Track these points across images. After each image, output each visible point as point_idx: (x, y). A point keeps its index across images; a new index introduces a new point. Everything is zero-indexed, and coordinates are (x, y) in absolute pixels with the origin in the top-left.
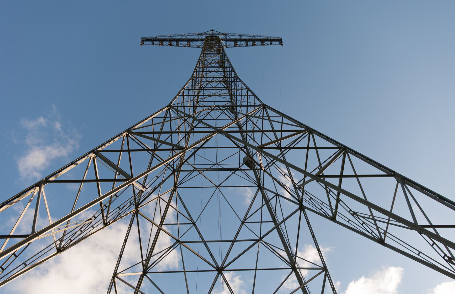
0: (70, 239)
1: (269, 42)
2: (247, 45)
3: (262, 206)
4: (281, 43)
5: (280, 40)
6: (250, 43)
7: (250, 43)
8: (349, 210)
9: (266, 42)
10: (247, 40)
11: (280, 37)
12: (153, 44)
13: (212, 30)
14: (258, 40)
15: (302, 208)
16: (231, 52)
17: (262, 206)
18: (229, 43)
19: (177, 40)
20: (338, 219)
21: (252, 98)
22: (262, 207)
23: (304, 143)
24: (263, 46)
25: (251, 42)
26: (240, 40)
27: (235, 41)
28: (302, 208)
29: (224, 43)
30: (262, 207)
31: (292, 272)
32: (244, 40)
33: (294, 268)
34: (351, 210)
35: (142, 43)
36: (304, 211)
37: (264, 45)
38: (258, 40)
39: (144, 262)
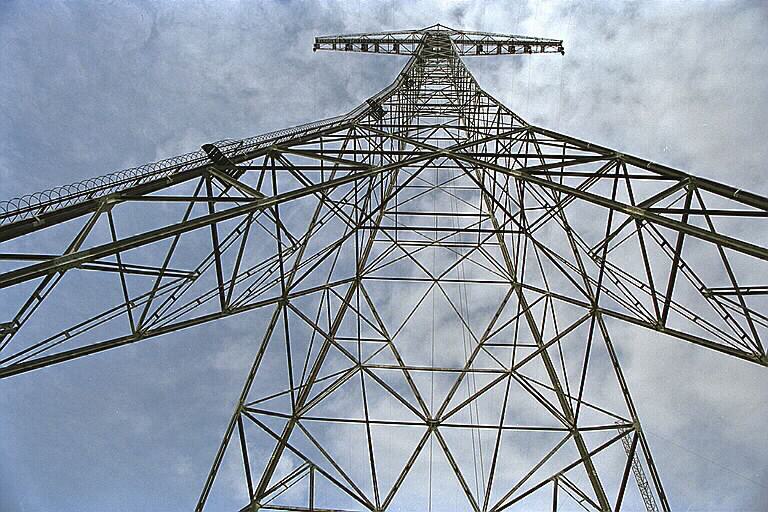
0: (158, 317)
1: (539, 48)
2: (499, 52)
3: (519, 315)
4: (561, 50)
5: (558, 45)
6: (505, 48)
7: (505, 48)
8: (700, 287)
9: (533, 48)
10: (500, 44)
11: (559, 39)
12: (335, 48)
13: (438, 25)
14: (519, 43)
15: (596, 312)
16: (471, 63)
17: (519, 315)
18: (467, 47)
19: (377, 42)
20: (673, 321)
21: (507, 119)
22: (517, 317)
23: (613, 172)
24: (528, 54)
25: (507, 47)
26: (488, 43)
27: (480, 45)
28: (596, 312)
29: (458, 48)
30: (517, 317)
31: (570, 436)
32: (494, 42)
33: (574, 431)
34: (704, 287)
35: (317, 47)
36: (600, 319)
37: (530, 52)
38: (519, 43)
39: (296, 392)
